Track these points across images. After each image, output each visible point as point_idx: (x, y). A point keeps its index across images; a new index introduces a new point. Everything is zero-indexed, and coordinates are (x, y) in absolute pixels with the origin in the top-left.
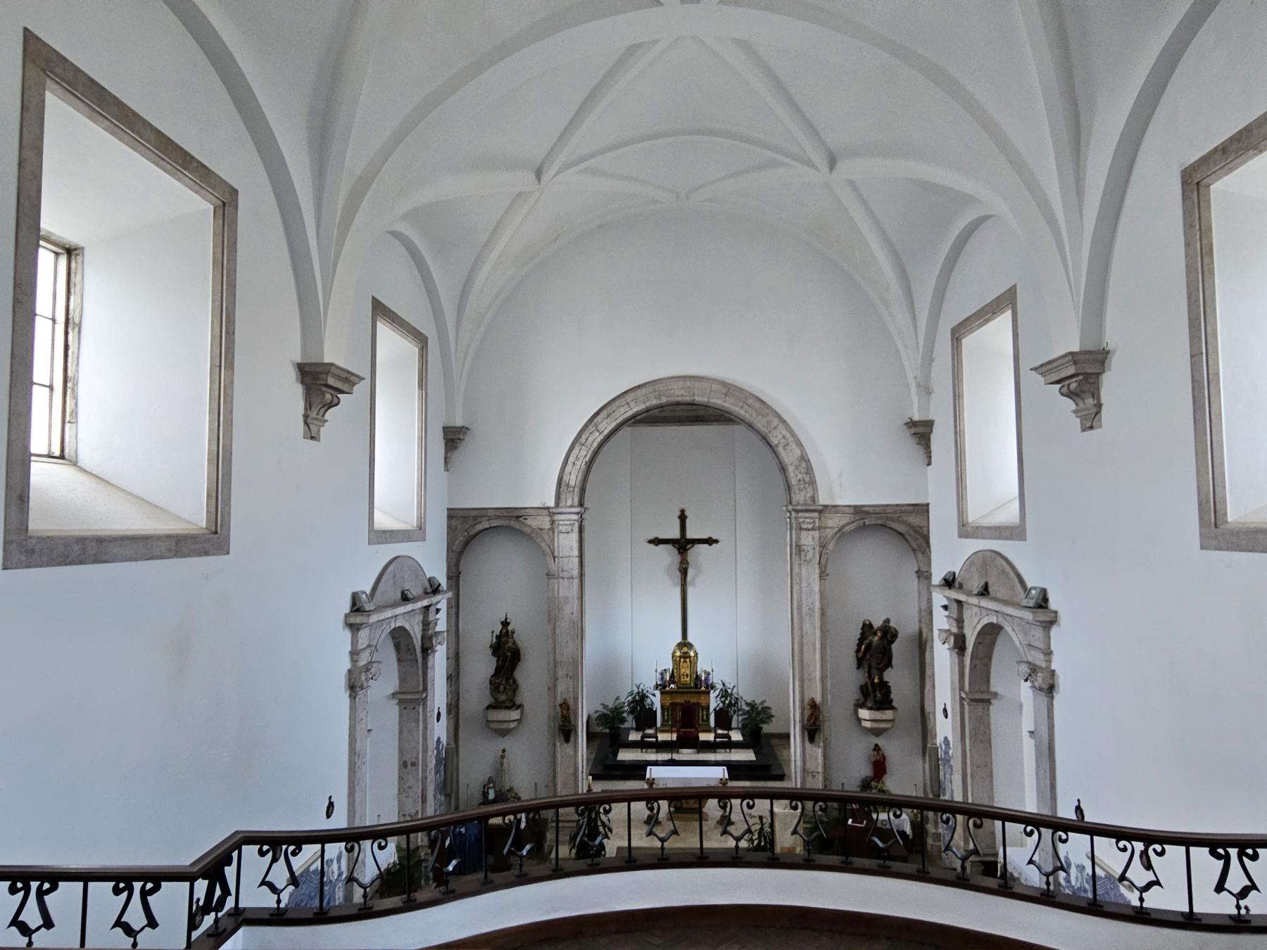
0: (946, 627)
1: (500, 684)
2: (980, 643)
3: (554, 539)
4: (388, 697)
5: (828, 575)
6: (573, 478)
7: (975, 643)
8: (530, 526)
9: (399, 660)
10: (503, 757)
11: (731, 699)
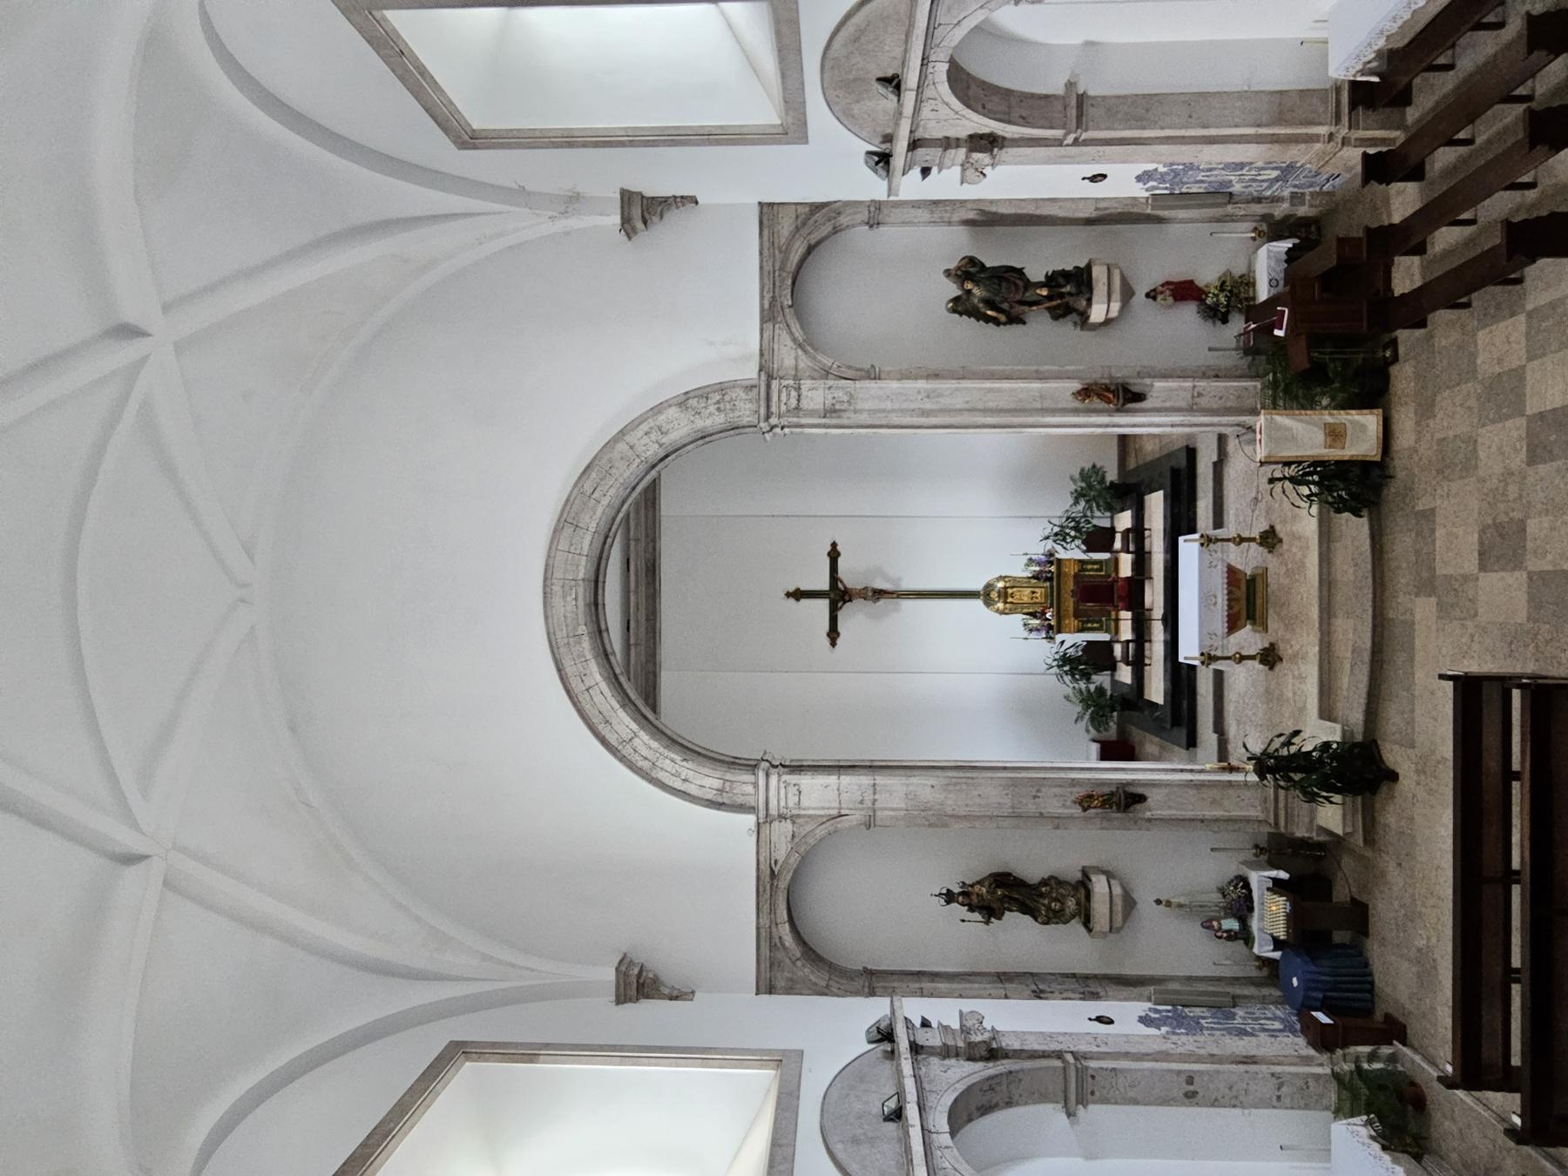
0: (957, 170)
1: (1049, 908)
2: (984, 107)
3: (809, 816)
4: (1072, 1124)
5: (872, 366)
6: (707, 780)
7: (984, 115)
8: (788, 857)
9: (1009, 1104)
10: (1169, 904)
11: (1068, 527)
